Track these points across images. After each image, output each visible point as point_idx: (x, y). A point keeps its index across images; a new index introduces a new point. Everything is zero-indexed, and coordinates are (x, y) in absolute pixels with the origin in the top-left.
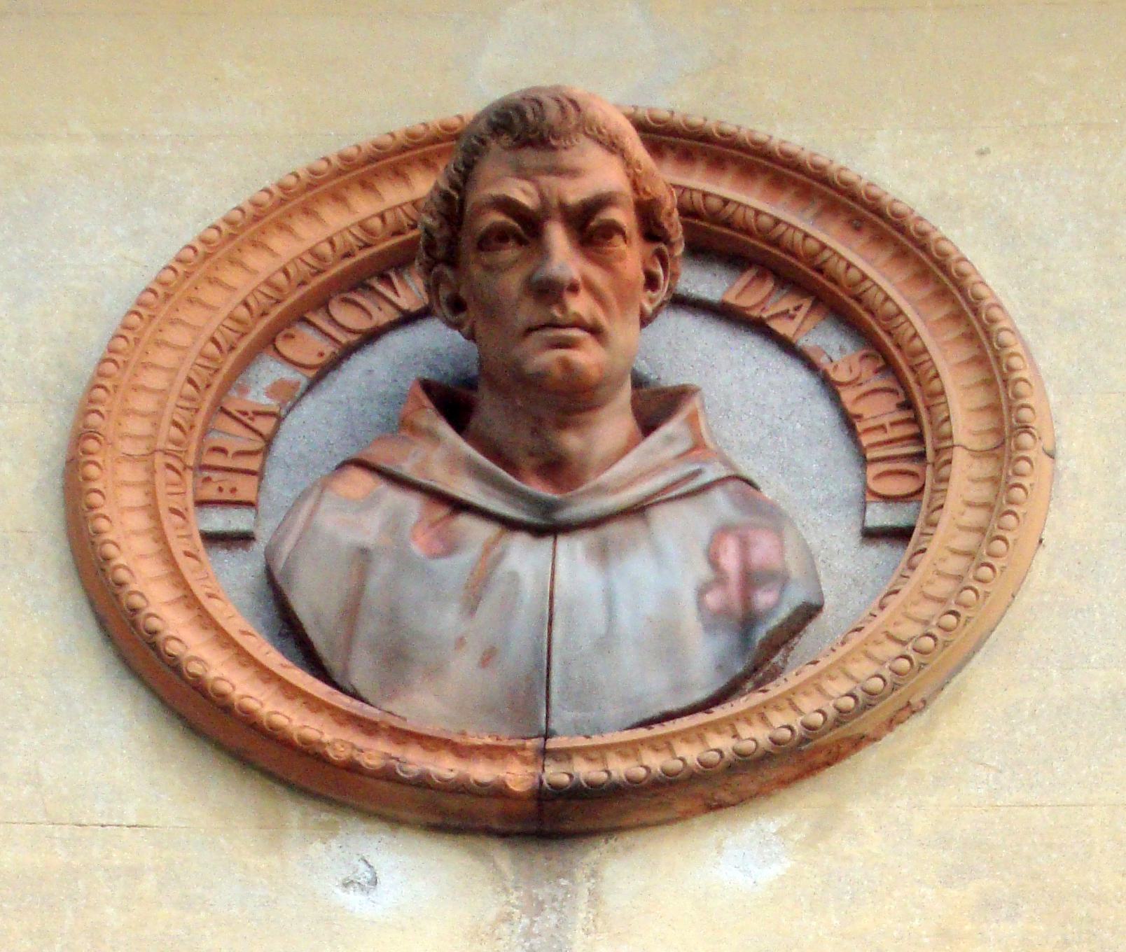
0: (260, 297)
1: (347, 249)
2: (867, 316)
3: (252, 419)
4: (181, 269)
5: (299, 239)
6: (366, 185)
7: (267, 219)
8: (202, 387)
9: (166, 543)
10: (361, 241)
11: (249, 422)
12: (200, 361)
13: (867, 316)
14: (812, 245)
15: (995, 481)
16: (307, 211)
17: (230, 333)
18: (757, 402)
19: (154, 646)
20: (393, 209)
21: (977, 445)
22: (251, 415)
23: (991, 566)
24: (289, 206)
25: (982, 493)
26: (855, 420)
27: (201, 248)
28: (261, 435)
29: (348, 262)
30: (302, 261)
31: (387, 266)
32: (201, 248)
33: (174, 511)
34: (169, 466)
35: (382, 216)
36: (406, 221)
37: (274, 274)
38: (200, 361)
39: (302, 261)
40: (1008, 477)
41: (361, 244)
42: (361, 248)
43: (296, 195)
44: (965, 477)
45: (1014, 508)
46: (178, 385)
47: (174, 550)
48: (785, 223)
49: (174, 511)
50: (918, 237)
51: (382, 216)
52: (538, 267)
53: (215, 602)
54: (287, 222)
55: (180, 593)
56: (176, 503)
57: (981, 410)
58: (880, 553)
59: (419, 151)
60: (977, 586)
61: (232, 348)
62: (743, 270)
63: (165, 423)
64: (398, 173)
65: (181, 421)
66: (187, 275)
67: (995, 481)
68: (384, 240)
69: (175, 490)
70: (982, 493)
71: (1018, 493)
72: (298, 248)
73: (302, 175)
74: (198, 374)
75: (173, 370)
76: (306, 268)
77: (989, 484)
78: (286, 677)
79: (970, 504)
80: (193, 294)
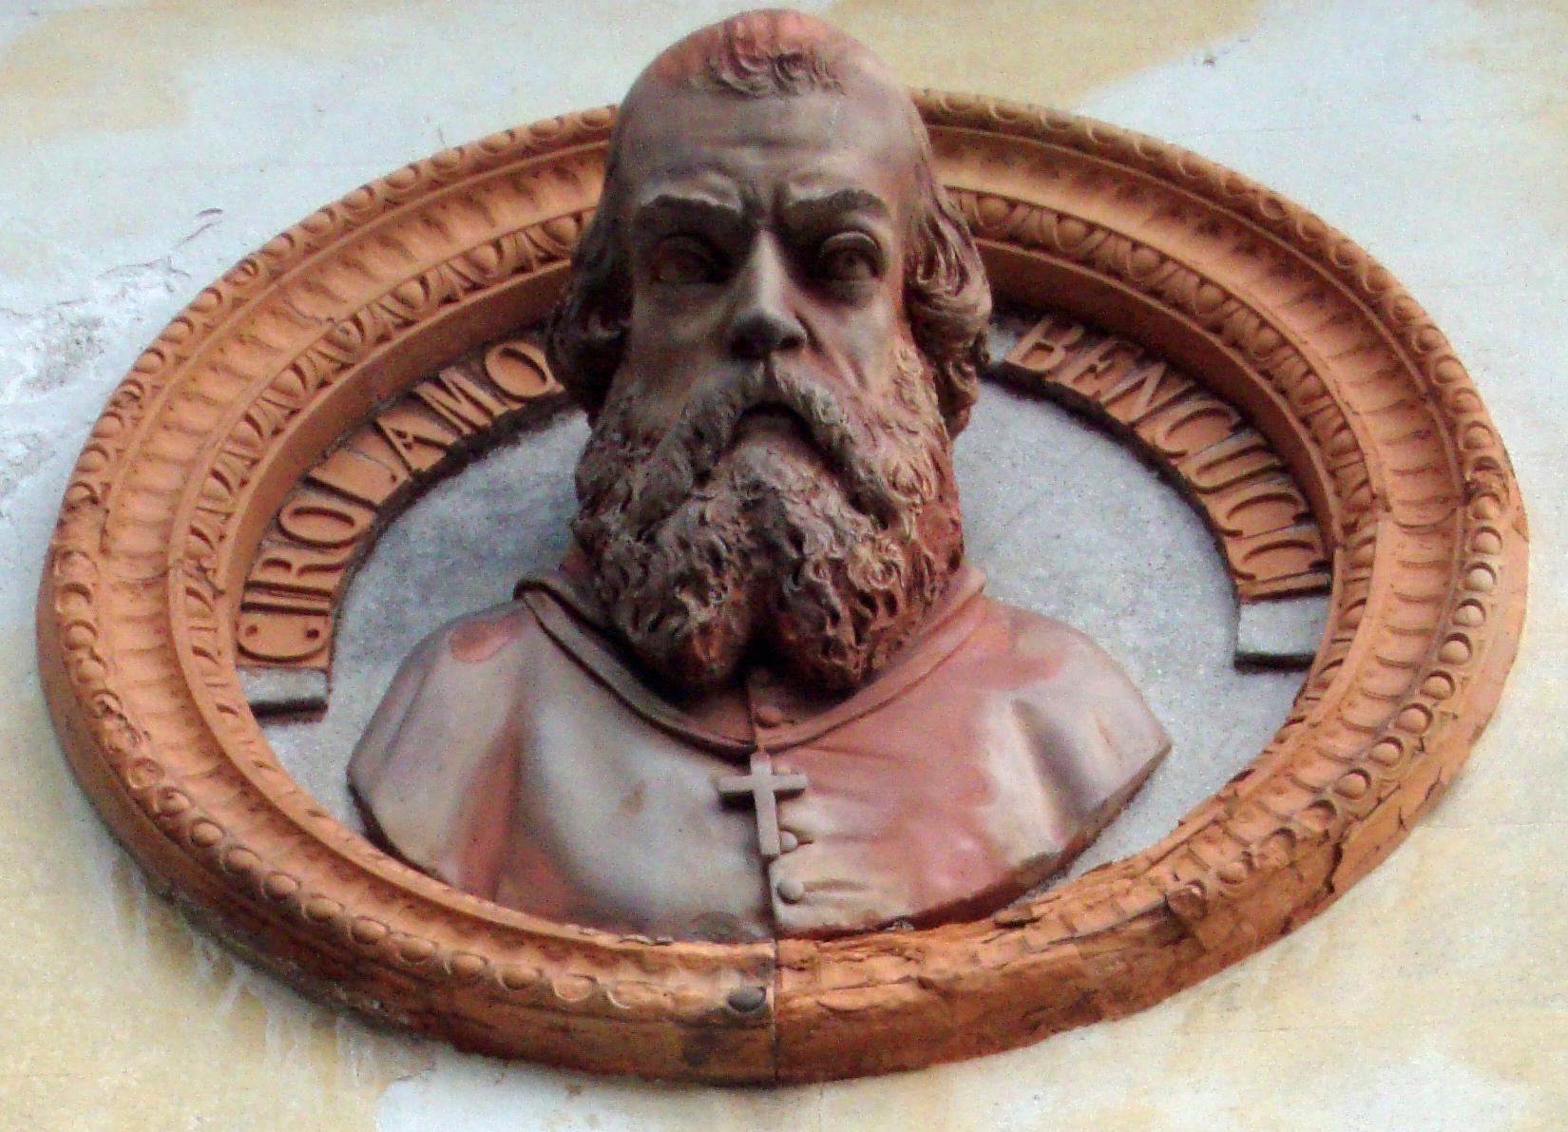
0: (314, 356)
1: (380, 331)
2: (1277, 399)
3: (408, 446)
4: (198, 319)
5: (335, 299)
6: (472, 202)
7: (407, 207)
8: (233, 482)
9: (189, 695)
10: (466, 278)
11: (403, 451)
12: (229, 447)
13: (1277, 399)
14: (1146, 257)
15: (1441, 566)
16: (349, 263)
17: (273, 408)
18: (1067, 532)
19: (174, 835)
20: (512, 234)
21: (1411, 517)
22: (410, 439)
23: (1448, 677)
24: (357, 233)
25: (1425, 583)
26: (1227, 539)
27: (227, 291)
28: (409, 468)
29: (384, 348)
30: (383, 307)
31: (471, 341)
32: (227, 291)
33: (199, 652)
34: (190, 592)
35: (578, 217)
36: (279, 414)
37: (407, 281)
38: (229, 447)
39: (383, 307)
40: (1464, 554)
41: (398, 321)
42: (467, 291)
43: (368, 216)
44: (1394, 557)
45: (1477, 596)
46: (193, 490)
47: (200, 703)
48: (1104, 229)
49: (199, 652)
50: (1307, 239)
51: (497, 245)
52: (732, 308)
53: (265, 772)
54: (359, 256)
55: (208, 766)
56: (205, 641)
57: (1420, 471)
58: (1272, 693)
59: (549, 156)
60: (1428, 703)
61: (277, 432)
62: (1034, 322)
63: (181, 536)
64: (519, 186)
65: (226, 474)
66: (208, 328)
67: (1441, 566)
68: (501, 280)
69: (198, 622)
70: (1425, 583)
71: (1481, 577)
72: (448, 250)
73: (377, 190)
74: (225, 463)
75: (189, 465)
76: (386, 316)
77: (1434, 572)
78: (377, 872)
79: (1407, 600)
80: (218, 357)
